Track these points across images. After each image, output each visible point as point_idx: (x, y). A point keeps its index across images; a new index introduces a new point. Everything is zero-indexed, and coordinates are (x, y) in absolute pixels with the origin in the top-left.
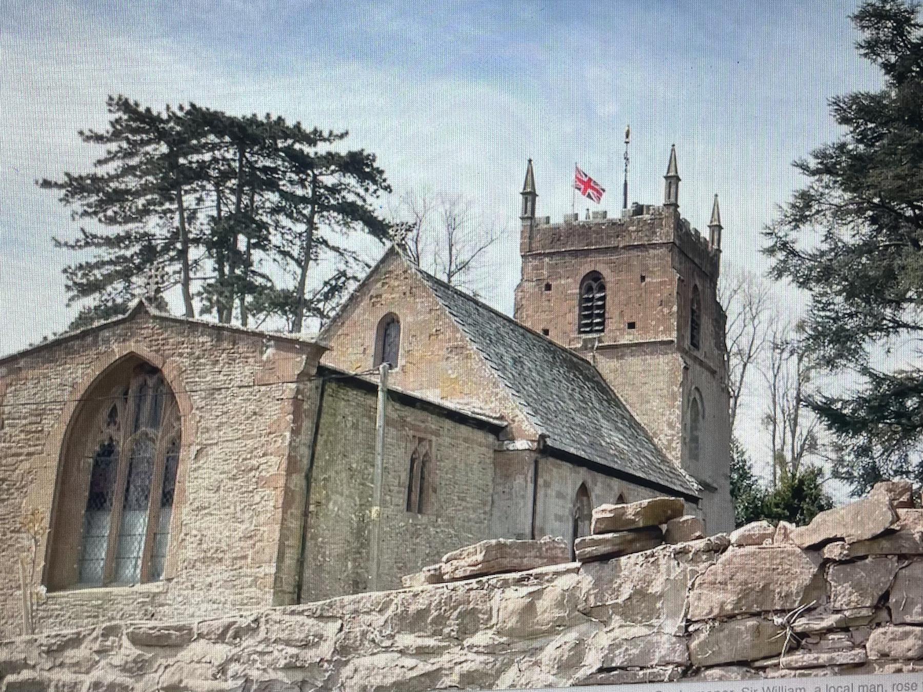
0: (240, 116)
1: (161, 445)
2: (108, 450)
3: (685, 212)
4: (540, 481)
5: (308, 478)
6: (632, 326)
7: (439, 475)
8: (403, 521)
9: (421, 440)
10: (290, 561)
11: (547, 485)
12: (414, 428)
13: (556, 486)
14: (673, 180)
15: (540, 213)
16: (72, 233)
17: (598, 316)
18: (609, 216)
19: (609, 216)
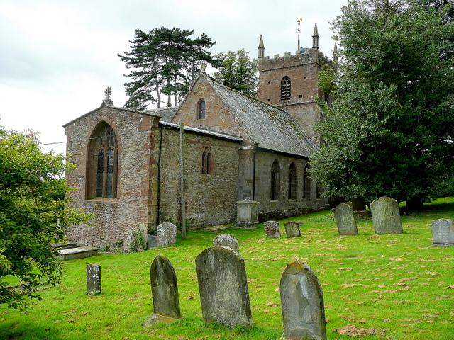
0: (170, 28)
1: (112, 154)
2: (101, 153)
3: (321, 50)
4: (256, 160)
5: (159, 165)
6: (301, 96)
7: (214, 158)
8: (201, 177)
9: (206, 148)
10: (154, 194)
11: (259, 161)
12: (203, 144)
13: (263, 162)
14: (316, 37)
15: (266, 55)
16: (129, 72)
17: (288, 93)
18: (291, 54)
19: (291, 54)
